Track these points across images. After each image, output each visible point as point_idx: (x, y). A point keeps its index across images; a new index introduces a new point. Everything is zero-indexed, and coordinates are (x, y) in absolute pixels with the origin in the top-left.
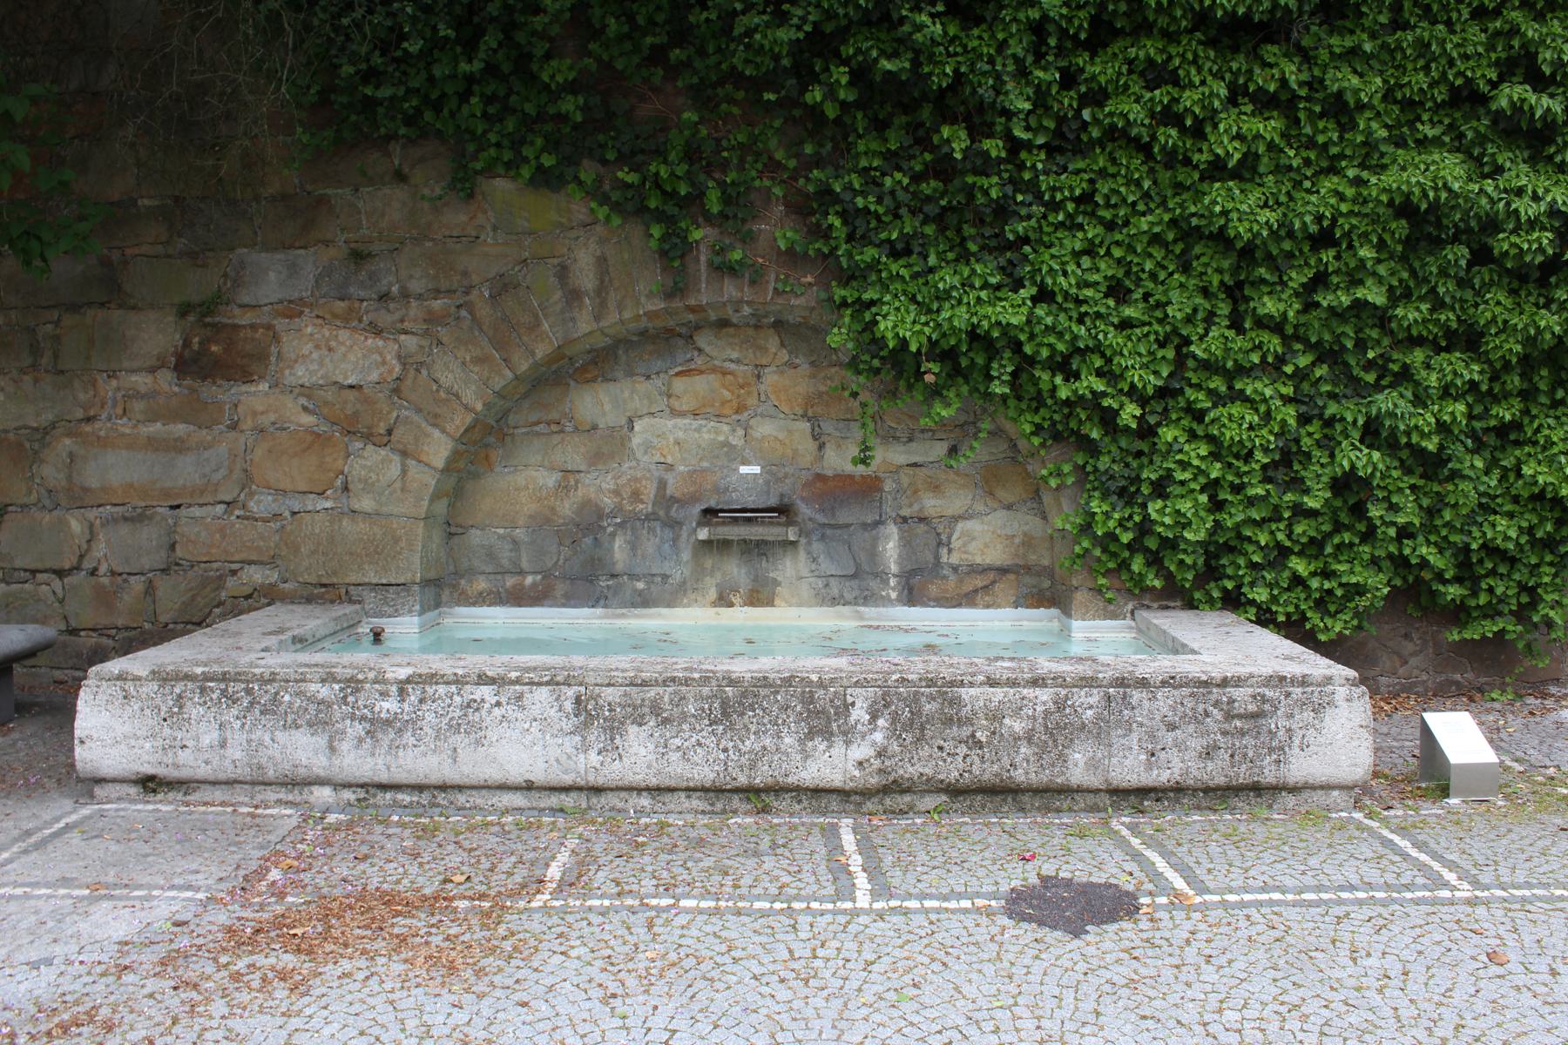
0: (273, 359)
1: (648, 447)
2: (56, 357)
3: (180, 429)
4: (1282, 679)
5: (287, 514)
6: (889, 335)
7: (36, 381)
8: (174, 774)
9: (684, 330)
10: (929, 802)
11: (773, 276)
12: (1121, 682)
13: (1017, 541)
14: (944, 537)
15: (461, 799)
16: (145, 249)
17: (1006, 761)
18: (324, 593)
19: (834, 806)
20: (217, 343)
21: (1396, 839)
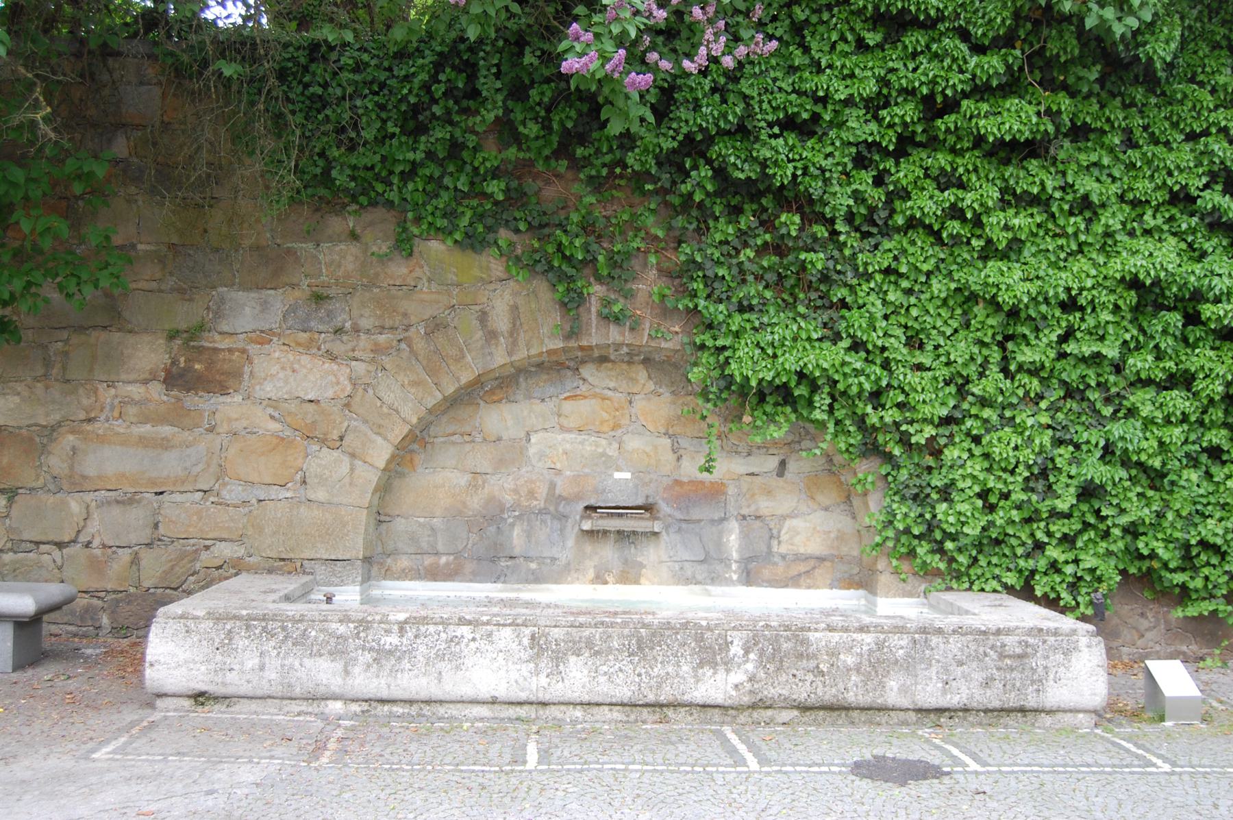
0: (246, 377)
1: (542, 456)
2: (64, 368)
3: (166, 430)
4: (1041, 630)
5: (254, 501)
6: (737, 373)
7: (47, 388)
8: (221, 690)
9: (572, 364)
10: (786, 715)
11: (648, 325)
12: (924, 630)
13: (832, 535)
14: (775, 532)
15: (441, 710)
16: (141, 285)
17: (841, 686)
18: (283, 565)
19: (717, 718)
20: (199, 362)
21: (1123, 743)
